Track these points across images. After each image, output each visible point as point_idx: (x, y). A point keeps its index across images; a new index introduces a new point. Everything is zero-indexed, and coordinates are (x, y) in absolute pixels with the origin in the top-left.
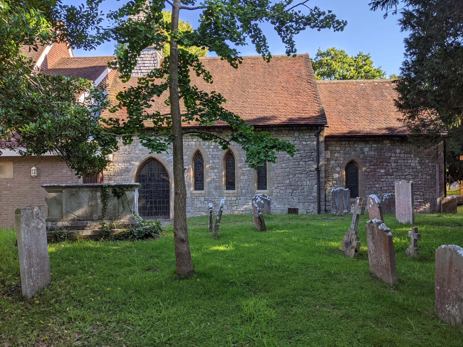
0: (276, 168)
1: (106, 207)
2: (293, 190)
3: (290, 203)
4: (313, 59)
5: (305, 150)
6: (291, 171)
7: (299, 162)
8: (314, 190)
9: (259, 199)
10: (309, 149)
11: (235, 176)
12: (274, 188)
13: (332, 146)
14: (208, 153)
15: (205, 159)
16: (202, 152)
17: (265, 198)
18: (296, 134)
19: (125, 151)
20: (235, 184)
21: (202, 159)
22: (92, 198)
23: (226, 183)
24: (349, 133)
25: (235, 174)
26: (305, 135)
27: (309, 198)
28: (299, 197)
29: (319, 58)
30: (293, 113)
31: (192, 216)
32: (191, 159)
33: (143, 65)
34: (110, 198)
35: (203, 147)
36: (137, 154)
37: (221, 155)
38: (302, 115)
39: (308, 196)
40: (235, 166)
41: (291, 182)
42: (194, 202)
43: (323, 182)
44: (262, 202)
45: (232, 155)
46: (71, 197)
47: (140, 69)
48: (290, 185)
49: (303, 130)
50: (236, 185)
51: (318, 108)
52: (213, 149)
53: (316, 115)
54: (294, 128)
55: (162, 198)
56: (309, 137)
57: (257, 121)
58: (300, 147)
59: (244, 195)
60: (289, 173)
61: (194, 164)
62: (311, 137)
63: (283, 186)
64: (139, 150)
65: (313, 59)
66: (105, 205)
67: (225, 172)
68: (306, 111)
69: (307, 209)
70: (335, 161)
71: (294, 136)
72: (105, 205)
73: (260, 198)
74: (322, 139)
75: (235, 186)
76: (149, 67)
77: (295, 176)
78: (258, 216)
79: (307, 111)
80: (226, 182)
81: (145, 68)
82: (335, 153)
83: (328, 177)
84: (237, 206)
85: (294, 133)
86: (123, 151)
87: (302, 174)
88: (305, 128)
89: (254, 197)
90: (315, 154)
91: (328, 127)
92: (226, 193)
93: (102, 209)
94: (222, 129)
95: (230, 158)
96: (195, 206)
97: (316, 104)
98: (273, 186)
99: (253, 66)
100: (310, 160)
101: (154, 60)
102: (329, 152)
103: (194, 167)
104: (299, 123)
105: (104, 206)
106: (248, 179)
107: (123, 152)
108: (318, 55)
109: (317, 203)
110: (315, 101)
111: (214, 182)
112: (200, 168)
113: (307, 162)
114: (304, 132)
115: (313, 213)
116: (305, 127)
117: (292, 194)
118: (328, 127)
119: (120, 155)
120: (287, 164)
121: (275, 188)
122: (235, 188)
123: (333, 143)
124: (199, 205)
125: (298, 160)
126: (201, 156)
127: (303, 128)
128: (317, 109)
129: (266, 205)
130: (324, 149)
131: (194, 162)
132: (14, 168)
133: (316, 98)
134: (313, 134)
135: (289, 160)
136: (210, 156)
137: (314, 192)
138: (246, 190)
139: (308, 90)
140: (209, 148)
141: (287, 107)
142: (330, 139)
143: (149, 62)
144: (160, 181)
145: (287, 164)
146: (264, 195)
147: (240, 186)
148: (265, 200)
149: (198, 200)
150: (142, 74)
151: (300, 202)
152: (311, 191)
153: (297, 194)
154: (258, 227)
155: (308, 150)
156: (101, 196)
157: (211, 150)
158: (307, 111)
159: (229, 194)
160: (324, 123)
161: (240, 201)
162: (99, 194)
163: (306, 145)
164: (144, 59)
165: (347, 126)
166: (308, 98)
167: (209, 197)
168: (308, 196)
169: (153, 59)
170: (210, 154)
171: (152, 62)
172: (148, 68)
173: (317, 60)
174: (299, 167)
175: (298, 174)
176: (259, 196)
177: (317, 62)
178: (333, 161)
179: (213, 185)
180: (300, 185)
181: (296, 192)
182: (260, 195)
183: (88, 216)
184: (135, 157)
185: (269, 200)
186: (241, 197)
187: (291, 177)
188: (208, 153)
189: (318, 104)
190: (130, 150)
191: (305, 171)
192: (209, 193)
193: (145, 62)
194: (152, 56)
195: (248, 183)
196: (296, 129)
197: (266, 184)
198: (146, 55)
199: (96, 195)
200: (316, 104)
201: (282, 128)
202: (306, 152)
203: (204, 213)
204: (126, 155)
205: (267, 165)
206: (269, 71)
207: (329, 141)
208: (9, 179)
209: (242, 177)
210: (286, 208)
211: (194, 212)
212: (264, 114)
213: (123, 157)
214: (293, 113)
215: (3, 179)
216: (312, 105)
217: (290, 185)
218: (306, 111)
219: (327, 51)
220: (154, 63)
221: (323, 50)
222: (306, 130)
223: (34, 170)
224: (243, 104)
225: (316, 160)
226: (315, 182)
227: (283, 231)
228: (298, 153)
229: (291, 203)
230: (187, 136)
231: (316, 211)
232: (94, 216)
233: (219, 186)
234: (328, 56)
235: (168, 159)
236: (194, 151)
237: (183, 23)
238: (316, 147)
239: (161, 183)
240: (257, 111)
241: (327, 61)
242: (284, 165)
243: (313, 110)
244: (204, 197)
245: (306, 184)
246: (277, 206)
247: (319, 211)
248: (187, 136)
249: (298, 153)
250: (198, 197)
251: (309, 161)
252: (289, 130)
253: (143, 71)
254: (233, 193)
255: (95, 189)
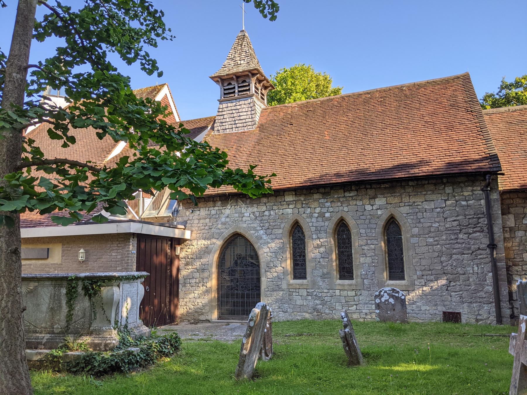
0: (417, 245)
1: (72, 312)
2: (450, 282)
3: (446, 303)
4: (495, 94)
5: (465, 215)
6: (444, 249)
7: (457, 234)
8: (488, 281)
9: (386, 297)
10: (473, 213)
11: (352, 258)
12: (415, 277)
13: (516, 206)
14: (311, 224)
15: (307, 234)
16: (302, 223)
17: (397, 295)
18: (449, 190)
19: (205, 226)
20: (353, 270)
21: (303, 233)
22: (54, 297)
23: (340, 269)
24: (374, 198)
25: (351, 256)
26: (464, 190)
27: (478, 294)
28: (461, 293)
29: (504, 92)
30: (442, 158)
31: (290, 317)
32: (287, 234)
33: (238, 118)
34: (78, 298)
35: (303, 215)
36: (219, 229)
37: (329, 226)
38: (456, 159)
39: (476, 291)
40: (351, 242)
41: (446, 268)
42: (293, 298)
43: (503, 268)
44: (391, 300)
45: (347, 227)
46: (28, 295)
47: (235, 124)
48: (444, 273)
49: (460, 183)
50: (354, 271)
51: (485, 146)
52: (317, 218)
53: (481, 157)
54: (445, 180)
55: (252, 289)
56: (470, 193)
57: (382, 173)
58: (457, 209)
59: (367, 288)
60: (441, 254)
61: (291, 241)
62: (475, 192)
63: (432, 275)
64: (222, 224)
65: (495, 94)
66: (71, 307)
67: (337, 252)
68: (464, 153)
69: (477, 313)
70: (524, 232)
71: (445, 192)
72: (71, 307)
73: (388, 294)
74: (495, 196)
75: (352, 273)
76: (245, 119)
77: (451, 257)
78: (343, 334)
79: (466, 153)
80: (340, 267)
81: (240, 122)
82: (523, 218)
83: (514, 258)
84: (356, 305)
85: (444, 188)
86: (203, 226)
87: (464, 254)
88: (463, 179)
89: (377, 293)
90: (484, 221)
91: (503, 174)
92: (339, 285)
93: (67, 315)
94: (329, 188)
95: (343, 231)
96: (294, 304)
97: (481, 141)
98: (414, 275)
99: (382, 100)
100: (476, 231)
101: (251, 111)
102: (511, 217)
103: (291, 245)
104: (452, 172)
105: (70, 311)
106: (373, 263)
107: (203, 227)
108: (502, 88)
109: (494, 304)
110: (480, 137)
111: (320, 268)
112: (300, 246)
113: (470, 234)
114: (462, 185)
115: (489, 322)
116: (462, 178)
117: (449, 288)
118: (503, 174)
119: (199, 232)
120: (436, 239)
121: (418, 278)
122: (353, 276)
123: (519, 201)
124: (299, 302)
125: (455, 232)
126: (301, 229)
127: (459, 179)
128: (483, 149)
129: (398, 307)
130: (500, 212)
131: (291, 237)
132: (63, 251)
133: (481, 133)
134: (479, 188)
135: (438, 231)
136: (313, 229)
137: (488, 285)
138: (370, 281)
139: (467, 123)
140: (311, 217)
141: (432, 150)
142: (512, 195)
143: (245, 114)
144: (249, 265)
145: (436, 239)
146: (393, 290)
147: (359, 274)
148: (396, 298)
149: (298, 294)
150: (237, 129)
151: (463, 302)
152: (483, 283)
153: (458, 288)
154: (346, 358)
155: (470, 215)
156: (67, 294)
157: (314, 220)
158: (466, 153)
159: (343, 285)
160: (495, 169)
161: (361, 298)
162: (64, 291)
163: (468, 206)
164: (240, 111)
165: (453, 130)
166: (467, 133)
167: (313, 290)
168: (476, 291)
169: (250, 109)
170: (313, 226)
171: (249, 113)
172: (244, 121)
173: (501, 94)
174: (457, 243)
175: (456, 254)
176: (385, 292)
177: (501, 97)
178: (520, 232)
179: (319, 272)
180: (461, 272)
181: (454, 284)
182: (387, 289)
183: (47, 326)
184: (217, 233)
185: (403, 297)
186: (363, 292)
187: (444, 259)
188: (311, 224)
189: (484, 141)
190: (211, 224)
191: (469, 249)
192: (314, 283)
193: (241, 114)
194: (250, 106)
195: (373, 269)
196: (448, 182)
197: (403, 271)
198: (243, 106)
199: (60, 293)
200: (481, 141)
201: (424, 182)
202: (468, 217)
203: (307, 314)
204: (207, 231)
205: (403, 241)
206: (405, 104)
207: (510, 198)
208: (57, 264)
209: (362, 260)
210: (439, 311)
211: (293, 312)
212: (393, 163)
213: (203, 234)
214: (442, 158)
215: (52, 264)
216: (474, 143)
217: (444, 273)
218: (464, 153)
219: (516, 81)
220: (251, 114)
221: (510, 80)
222: (466, 181)
223: (82, 253)
224: (363, 151)
225: (487, 231)
226: (488, 267)
227: (387, 368)
228: (455, 221)
229: (447, 303)
230: (280, 202)
231: (493, 318)
232: (55, 327)
233: (328, 273)
234: (518, 87)
235: (256, 235)
236: (291, 222)
237: (320, 75)
238: (484, 210)
239: (250, 268)
240: (384, 159)
241: (516, 94)
242: (431, 240)
243: (476, 150)
244: (307, 289)
245: (471, 271)
246: (423, 308)
247: (500, 319)
248: (280, 202)
249: (455, 221)
250: (297, 289)
251: (474, 232)
252: (435, 184)
253: (238, 125)
254: (350, 285)
255: (59, 282)
